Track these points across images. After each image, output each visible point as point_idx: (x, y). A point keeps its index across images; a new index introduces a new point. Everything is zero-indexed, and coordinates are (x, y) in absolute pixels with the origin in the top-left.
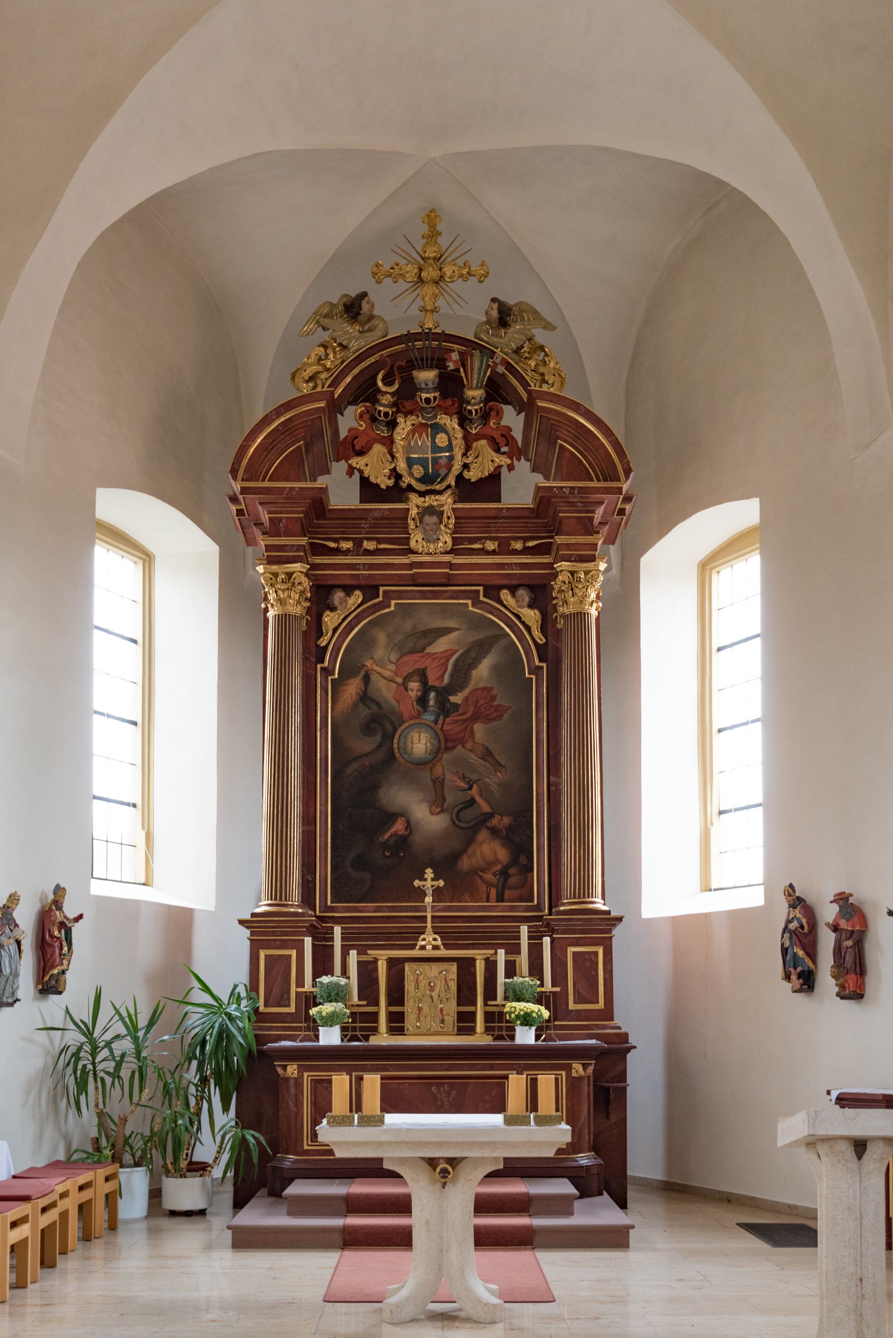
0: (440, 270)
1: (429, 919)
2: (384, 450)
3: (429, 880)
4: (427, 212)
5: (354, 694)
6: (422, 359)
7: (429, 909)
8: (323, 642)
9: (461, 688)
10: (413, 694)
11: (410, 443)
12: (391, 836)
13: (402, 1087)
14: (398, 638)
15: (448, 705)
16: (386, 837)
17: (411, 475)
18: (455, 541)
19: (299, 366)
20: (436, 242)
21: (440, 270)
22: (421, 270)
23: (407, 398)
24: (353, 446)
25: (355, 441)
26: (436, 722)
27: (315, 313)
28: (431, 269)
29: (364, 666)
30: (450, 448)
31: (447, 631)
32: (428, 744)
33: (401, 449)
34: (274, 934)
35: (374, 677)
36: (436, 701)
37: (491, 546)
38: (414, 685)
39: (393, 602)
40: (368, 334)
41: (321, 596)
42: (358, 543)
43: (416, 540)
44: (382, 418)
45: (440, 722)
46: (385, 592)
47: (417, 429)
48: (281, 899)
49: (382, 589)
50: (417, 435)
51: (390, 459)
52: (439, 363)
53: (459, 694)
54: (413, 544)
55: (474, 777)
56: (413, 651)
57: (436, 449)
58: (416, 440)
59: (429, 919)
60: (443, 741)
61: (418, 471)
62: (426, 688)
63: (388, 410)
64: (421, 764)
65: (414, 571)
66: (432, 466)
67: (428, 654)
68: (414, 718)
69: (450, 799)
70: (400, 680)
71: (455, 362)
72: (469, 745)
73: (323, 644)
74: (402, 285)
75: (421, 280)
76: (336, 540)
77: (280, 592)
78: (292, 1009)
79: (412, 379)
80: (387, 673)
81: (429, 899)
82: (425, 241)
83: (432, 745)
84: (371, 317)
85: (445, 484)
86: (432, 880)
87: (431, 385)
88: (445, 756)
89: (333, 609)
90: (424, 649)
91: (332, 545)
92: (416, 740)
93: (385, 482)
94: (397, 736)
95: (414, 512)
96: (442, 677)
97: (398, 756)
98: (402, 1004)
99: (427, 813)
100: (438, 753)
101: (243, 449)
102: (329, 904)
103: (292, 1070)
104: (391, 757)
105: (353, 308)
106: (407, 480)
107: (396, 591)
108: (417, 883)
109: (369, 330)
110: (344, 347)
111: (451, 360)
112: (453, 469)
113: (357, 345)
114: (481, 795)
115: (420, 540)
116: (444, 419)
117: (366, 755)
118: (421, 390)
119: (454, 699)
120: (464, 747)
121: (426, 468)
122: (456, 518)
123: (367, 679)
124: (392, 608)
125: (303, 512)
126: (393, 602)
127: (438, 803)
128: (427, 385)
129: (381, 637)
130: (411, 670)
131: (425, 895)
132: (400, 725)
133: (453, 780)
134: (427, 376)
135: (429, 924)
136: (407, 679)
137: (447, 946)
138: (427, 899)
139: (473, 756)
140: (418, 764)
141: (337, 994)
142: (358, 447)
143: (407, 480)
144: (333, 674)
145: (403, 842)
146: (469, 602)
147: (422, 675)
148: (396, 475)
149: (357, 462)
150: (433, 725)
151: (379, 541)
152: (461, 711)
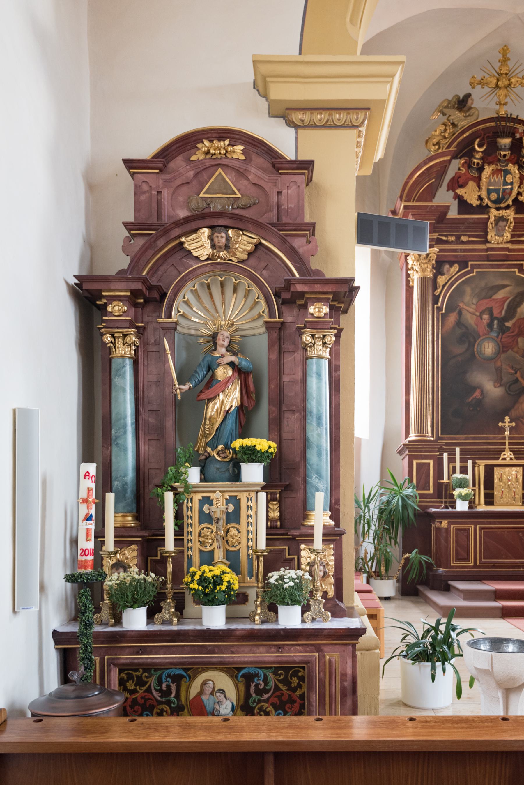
0: (509, 80)
1: (507, 444)
2: (475, 184)
3: (507, 423)
4: (502, 47)
5: (453, 322)
6: (504, 132)
7: (507, 438)
8: (437, 293)
9: (512, 318)
10: (485, 321)
11: (491, 180)
12: (473, 399)
13: (503, 533)
14: (477, 290)
15: (504, 328)
16: (470, 400)
17: (489, 198)
18: (513, 236)
19: (430, 136)
20: (507, 65)
21: (509, 80)
22: (498, 80)
23: (491, 154)
24: (458, 182)
25: (459, 179)
26: (497, 337)
27: (439, 106)
28: (504, 80)
29: (459, 306)
30: (512, 184)
31: (504, 286)
32: (493, 349)
33: (485, 184)
34: (421, 451)
35: (464, 312)
36: (498, 324)
37: (453, 239)
38: (486, 317)
39: (475, 270)
40: (469, 118)
41: (439, 267)
42: (458, 237)
43: (491, 235)
44: (475, 166)
45: (500, 337)
46: (471, 265)
47: (494, 173)
48: (423, 433)
49: (470, 263)
50: (495, 176)
51: (478, 189)
52: (511, 134)
53: (510, 322)
54: (489, 237)
55: (518, 367)
56: (485, 298)
57: (505, 183)
58: (495, 179)
59: (507, 444)
60: (501, 347)
61: (494, 196)
62: (492, 318)
63: (479, 161)
64: (489, 360)
65: (489, 253)
66: (502, 193)
67: (494, 299)
68: (486, 335)
69: (505, 379)
70: (478, 314)
71: (520, 134)
72: (515, 349)
73: (437, 294)
74: (487, 89)
75: (497, 86)
76: (446, 236)
77: (422, 264)
78: (431, 491)
79: (496, 142)
80: (471, 310)
81: (507, 433)
82: (500, 63)
83: (495, 349)
84: (470, 108)
85: (506, 204)
86: (509, 422)
87: (507, 147)
88: (503, 356)
89: (443, 274)
90: (491, 297)
91: (444, 238)
92: (486, 347)
93: (475, 203)
94: (476, 344)
95: (492, 219)
96: (501, 312)
97: (477, 355)
98: (493, 489)
99: (493, 387)
100: (498, 354)
101: (406, 183)
102: (440, 435)
103: (445, 524)
104: (473, 356)
105: (462, 103)
106: (486, 201)
107: (477, 264)
108: (500, 424)
109: (469, 116)
110: (454, 125)
111: (518, 132)
112: (512, 195)
113: (464, 123)
114: (522, 377)
115: (493, 235)
116: (510, 167)
117: (460, 355)
118: (501, 150)
119: (507, 324)
120: (513, 351)
121: (498, 195)
122: (515, 223)
123: (460, 313)
124: (475, 274)
125: (435, 220)
126: (475, 270)
127: (499, 381)
128: (505, 146)
129: (468, 290)
130: (484, 308)
131: (505, 431)
132: (478, 339)
133: (507, 369)
134: (506, 141)
135: (507, 446)
136: (482, 313)
137: (517, 458)
138: (506, 433)
139: (517, 355)
140: (487, 360)
141: (464, 484)
142: (460, 183)
143: (486, 201)
144: (442, 311)
145: (479, 402)
146: (516, 270)
147: (490, 311)
148: (480, 198)
149: (460, 191)
150: (496, 339)
151: (470, 236)
152: (511, 330)
